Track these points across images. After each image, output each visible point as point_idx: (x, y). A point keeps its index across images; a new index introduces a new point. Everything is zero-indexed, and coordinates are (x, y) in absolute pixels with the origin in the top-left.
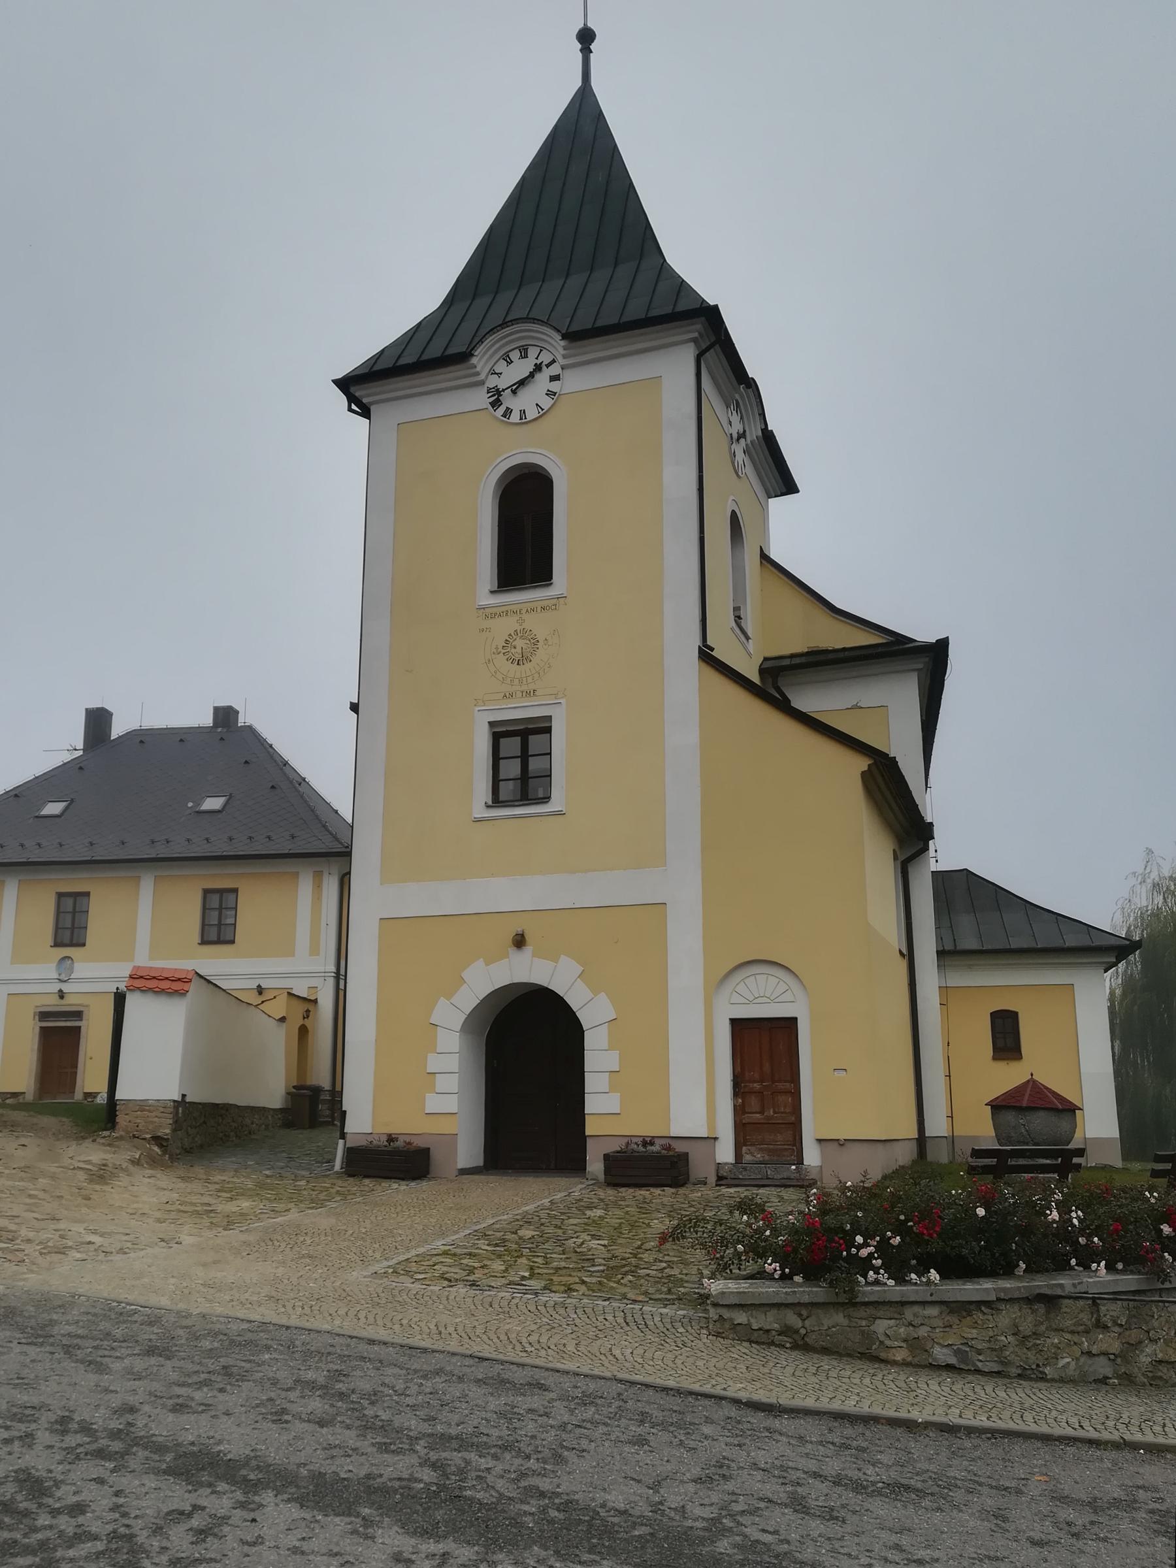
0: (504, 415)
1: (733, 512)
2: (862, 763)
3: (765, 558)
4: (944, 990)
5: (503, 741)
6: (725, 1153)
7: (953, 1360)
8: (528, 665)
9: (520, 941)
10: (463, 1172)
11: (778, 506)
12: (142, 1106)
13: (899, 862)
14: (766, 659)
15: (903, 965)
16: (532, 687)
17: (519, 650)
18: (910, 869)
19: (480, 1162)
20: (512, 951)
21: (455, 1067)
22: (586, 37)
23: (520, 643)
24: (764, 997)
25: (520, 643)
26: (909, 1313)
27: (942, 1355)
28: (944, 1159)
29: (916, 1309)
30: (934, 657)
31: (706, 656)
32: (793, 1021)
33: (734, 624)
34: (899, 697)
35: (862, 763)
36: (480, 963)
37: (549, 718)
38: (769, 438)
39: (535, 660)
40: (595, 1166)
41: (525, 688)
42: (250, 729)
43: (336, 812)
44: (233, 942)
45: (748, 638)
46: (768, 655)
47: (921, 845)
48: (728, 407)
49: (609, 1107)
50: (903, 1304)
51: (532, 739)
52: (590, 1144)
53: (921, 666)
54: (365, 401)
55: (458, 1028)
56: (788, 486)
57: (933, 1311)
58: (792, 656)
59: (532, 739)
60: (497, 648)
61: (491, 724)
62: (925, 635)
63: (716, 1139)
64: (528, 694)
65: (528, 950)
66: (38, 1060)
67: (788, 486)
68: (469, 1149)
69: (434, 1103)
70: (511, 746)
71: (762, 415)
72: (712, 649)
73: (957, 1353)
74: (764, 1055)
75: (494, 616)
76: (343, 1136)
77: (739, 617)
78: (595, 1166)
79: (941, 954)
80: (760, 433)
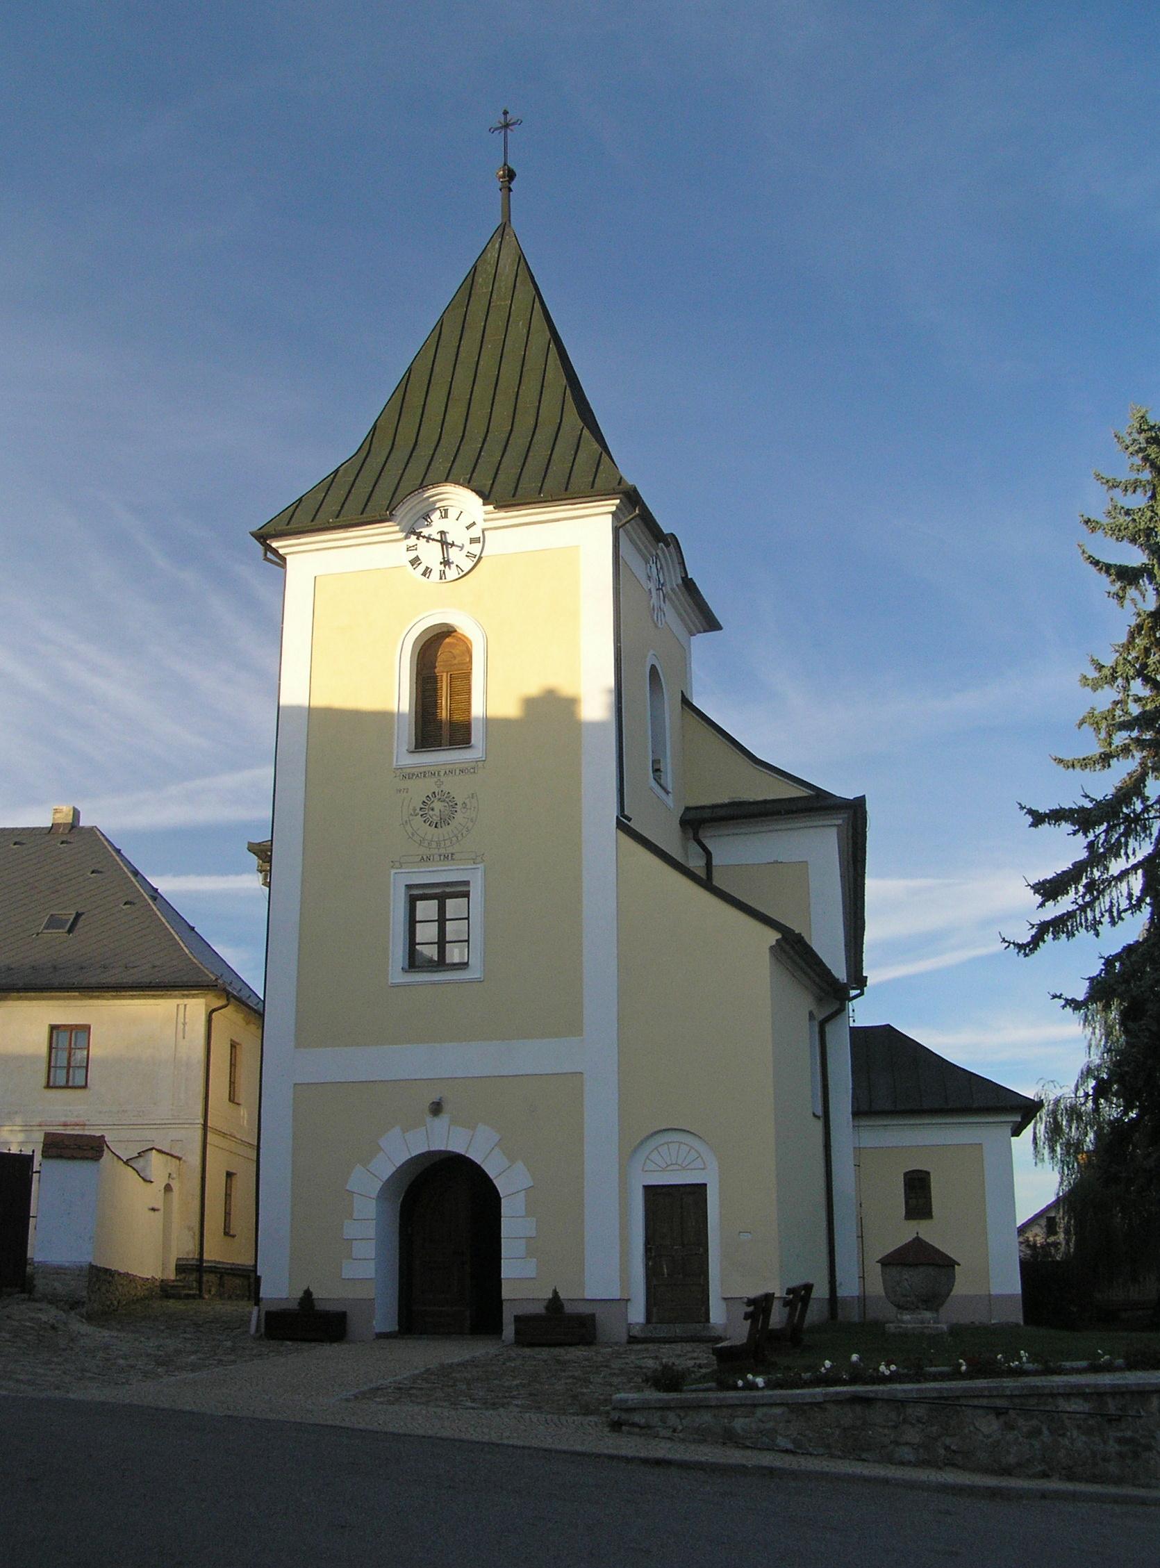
0: (424, 574)
1: (653, 668)
2: (773, 936)
3: (686, 703)
4: (858, 1150)
5: (420, 905)
6: (637, 1314)
7: (790, 1446)
8: (446, 829)
9: (436, 1108)
10: (380, 1336)
11: (701, 643)
12: (59, 1271)
13: (816, 1023)
14: (688, 809)
15: (819, 1125)
16: (450, 850)
17: (437, 812)
18: (827, 1029)
19: (395, 1328)
20: (429, 1118)
21: (372, 1233)
22: (510, 175)
23: (438, 806)
24: (672, 1166)
25: (438, 806)
26: (759, 1412)
27: (783, 1442)
28: (855, 1317)
29: (765, 1409)
30: (855, 811)
31: (623, 825)
32: (699, 1190)
33: (653, 783)
34: (819, 846)
35: (773, 936)
36: (397, 1130)
37: (467, 883)
38: (689, 586)
39: (454, 823)
40: (509, 1331)
41: (442, 851)
42: (92, 830)
43: (193, 929)
44: (85, 1087)
45: (668, 793)
46: (692, 803)
47: (836, 1006)
48: (647, 562)
49: (522, 1273)
50: (755, 1406)
51: (450, 903)
52: (506, 1307)
53: (840, 822)
54: (281, 551)
55: (374, 1194)
56: (711, 623)
57: (777, 1411)
58: (714, 807)
59: (450, 903)
60: (415, 810)
61: (409, 887)
62: (847, 792)
63: (628, 1300)
64: (446, 857)
65: (444, 1118)
66: (396, 1244)
67: (711, 623)
68: (384, 1317)
69: (350, 1270)
70: (427, 909)
71: (682, 563)
72: (629, 820)
73: (794, 1441)
74: (675, 1217)
75: (411, 776)
76: (257, 1301)
77: (658, 770)
78: (509, 1331)
79: (857, 1114)
80: (680, 581)
